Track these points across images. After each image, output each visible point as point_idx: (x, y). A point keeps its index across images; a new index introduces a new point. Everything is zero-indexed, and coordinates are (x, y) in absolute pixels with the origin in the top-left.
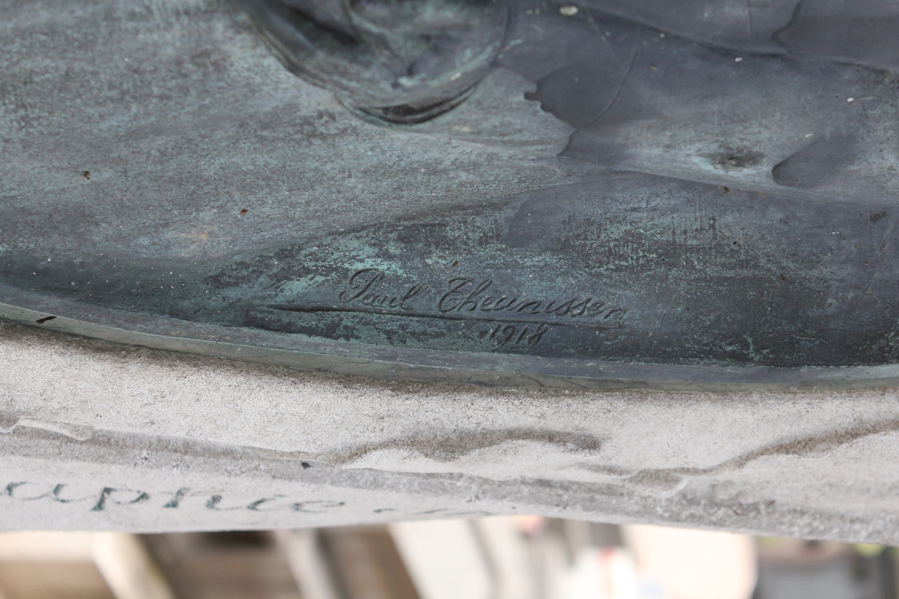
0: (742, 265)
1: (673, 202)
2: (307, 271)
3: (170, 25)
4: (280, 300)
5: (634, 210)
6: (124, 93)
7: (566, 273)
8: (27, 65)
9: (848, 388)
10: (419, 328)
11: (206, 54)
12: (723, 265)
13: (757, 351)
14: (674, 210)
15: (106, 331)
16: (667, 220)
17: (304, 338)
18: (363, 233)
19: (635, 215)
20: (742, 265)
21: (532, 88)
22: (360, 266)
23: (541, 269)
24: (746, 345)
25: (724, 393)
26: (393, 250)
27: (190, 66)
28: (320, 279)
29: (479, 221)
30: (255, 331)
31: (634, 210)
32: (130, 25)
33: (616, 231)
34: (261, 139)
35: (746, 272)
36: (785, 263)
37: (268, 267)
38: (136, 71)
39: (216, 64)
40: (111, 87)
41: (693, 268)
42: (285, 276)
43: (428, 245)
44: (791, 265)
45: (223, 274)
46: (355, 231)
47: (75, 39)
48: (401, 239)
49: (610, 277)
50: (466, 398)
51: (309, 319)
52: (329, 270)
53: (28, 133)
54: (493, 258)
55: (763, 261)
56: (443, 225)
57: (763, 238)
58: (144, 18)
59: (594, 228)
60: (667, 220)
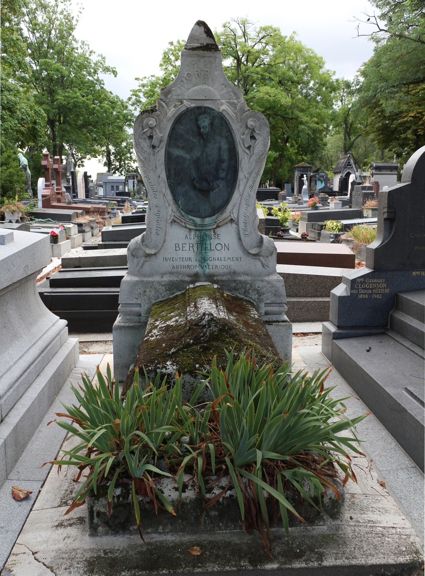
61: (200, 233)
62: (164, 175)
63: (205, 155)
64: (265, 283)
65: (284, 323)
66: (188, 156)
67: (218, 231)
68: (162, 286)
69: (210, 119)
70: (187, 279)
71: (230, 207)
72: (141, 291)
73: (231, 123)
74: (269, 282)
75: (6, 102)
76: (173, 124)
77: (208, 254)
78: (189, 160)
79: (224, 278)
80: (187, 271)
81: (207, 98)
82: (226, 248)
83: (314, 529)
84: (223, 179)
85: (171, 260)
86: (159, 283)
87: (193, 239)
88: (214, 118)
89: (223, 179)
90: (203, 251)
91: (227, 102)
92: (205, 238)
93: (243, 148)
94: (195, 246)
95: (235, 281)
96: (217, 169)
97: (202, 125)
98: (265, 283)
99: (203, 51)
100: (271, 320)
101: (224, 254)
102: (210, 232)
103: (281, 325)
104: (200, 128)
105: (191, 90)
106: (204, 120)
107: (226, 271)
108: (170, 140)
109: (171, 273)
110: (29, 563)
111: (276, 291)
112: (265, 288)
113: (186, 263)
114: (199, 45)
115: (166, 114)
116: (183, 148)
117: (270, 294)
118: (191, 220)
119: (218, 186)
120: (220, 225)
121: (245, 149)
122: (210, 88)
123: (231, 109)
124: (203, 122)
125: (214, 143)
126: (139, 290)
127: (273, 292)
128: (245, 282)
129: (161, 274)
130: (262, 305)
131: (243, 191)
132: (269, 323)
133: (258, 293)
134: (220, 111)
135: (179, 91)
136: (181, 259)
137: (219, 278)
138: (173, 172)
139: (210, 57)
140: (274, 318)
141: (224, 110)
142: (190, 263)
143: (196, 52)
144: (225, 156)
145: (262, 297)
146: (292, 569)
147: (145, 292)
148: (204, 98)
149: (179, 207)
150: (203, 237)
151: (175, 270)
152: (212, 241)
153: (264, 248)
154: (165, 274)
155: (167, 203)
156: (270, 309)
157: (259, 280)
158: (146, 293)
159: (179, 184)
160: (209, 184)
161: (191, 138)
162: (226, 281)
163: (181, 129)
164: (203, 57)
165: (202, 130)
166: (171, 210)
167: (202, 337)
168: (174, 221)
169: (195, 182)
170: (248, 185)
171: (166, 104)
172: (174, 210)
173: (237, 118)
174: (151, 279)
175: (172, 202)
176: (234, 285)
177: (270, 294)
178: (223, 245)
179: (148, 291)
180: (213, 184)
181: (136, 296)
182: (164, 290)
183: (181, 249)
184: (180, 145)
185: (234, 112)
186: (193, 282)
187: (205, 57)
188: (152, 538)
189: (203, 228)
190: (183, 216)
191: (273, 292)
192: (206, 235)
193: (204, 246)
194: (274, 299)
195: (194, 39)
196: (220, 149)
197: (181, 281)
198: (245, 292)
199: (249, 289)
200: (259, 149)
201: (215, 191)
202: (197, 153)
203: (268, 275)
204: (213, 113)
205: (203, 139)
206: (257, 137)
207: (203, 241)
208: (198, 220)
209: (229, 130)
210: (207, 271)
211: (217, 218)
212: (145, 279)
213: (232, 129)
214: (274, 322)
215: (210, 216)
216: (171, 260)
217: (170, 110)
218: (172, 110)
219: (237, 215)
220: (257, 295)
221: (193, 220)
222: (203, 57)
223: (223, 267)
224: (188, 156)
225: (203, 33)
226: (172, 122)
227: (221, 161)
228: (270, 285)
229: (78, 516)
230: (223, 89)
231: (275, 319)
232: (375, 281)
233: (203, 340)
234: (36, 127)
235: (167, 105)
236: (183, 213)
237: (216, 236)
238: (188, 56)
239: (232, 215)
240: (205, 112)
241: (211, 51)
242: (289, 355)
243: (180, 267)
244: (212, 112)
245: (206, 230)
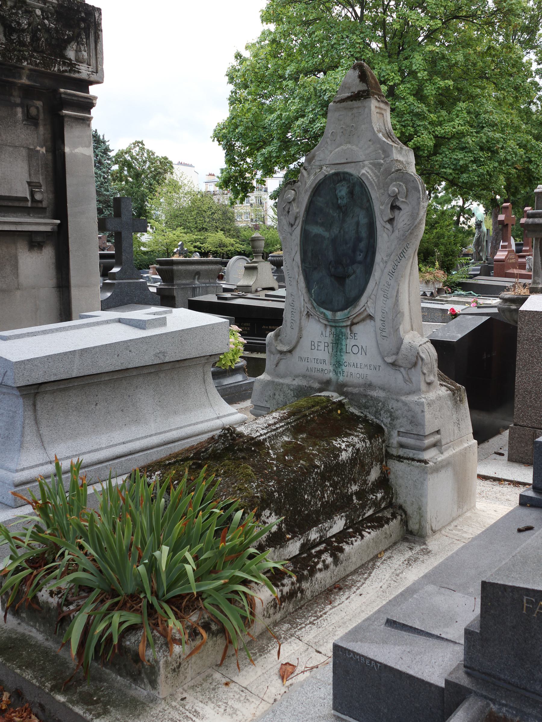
61: (336, 330)
62: (298, 258)
63: (342, 233)
64: (400, 404)
65: (419, 464)
66: (326, 234)
67: (356, 328)
68: (291, 390)
69: (348, 187)
70: (316, 385)
71: (363, 299)
72: (271, 393)
73: (370, 190)
74: (405, 404)
75: (484, 141)
76: (310, 196)
77: (344, 357)
78: (328, 238)
79: (356, 391)
80: (319, 375)
81: (349, 160)
82: (363, 353)
83: (136, 689)
84: (360, 263)
85: (306, 360)
86: (288, 385)
87: (327, 337)
88: (354, 185)
89: (360, 263)
90: (338, 353)
91: (371, 163)
92: (341, 336)
93: (382, 222)
94: (331, 345)
95: (366, 396)
96: (355, 249)
97: (339, 194)
98: (400, 404)
99: (352, 101)
100: (405, 456)
101: (360, 359)
102: (346, 330)
103: (413, 465)
105: (333, 153)
106: (341, 188)
107: (361, 381)
109: (304, 376)
111: (413, 417)
112: (399, 411)
113: (320, 366)
114: (349, 94)
116: (322, 225)
117: (405, 419)
118: (322, 313)
119: (354, 272)
120: (355, 321)
121: (384, 224)
122: (354, 147)
124: (340, 191)
125: (353, 217)
126: (269, 392)
127: (410, 417)
128: (377, 400)
129: (295, 376)
130: (395, 433)
131: (380, 278)
132: (400, 458)
133: (391, 416)
135: (322, 156)
136: (316, 360)
137: (350, 389)
138: (310, 255)
139: (358, 107)
140: (410, 453)
141: (363, 174)
142: (324, 367)
143: (344, 104)
144: (364, 233)
145: (394, 423)
146: (71, 710)
147: (275, 395)
148: (345, 161)
149: (311, 297)
150: (339, 336)
151: (308, 373)
152: (348, 341)
153: (400, 356)
154: (297, 376)
156: (404, 440)
157: (394, 399)
158: (275, 397)
159: (315, 269)
161: (331, 211)
162: (356, 394)
163: (320, 201)
164: (351, 109)
165: (339, 202)
167: (203, 452)
168: (308, 315)
169: (331, 267)
170: (386, 271)
172: (306, 300)
174: (281, 381)
175: (304, 290)
176: (364, 401)
177: (405, 419)
178: (360, 348)
179: (277, 394)
181: (267, 399)
182: (292, 395)
183: (316, 348)
184: (319, 221)
186: (321, 390)
187: (353, 108)
188: (31, 631)
189: (337, 325)
190: (314, 308)
191: (410, 417)
192: (342, 333)
193: (340, 346)
194: (409, 427)
195: (345, 88)
196: (358, 224)
197: (310, 387)
198: (376, 412)
199: (381, 409)
200: (404, 223)
201: (351, 278)
202: (335, 230)
203: (409, 393)
204: (352, 179)
206: (401, 206)
207: (338, 340)
208: (329, 314)
209: (369, 200)
210: (341, 378)
211: (349, 312)
212: (277, 380)
214: (408, 459)
215: (342, 310)
216: (306, 360)
220: (389, 419)
221: (324, 314)
222: (351, 109)
223: (358, 375)
224: (326, 234)
225: (357, 77)
226: (309, 193)
227: (359, 239)
228: (406, 408)
230: (369, 147)
231: (411, 455)
233: (203, 456)
234: (531, 167)
236: (315, 304)
237: (353, 335)
238: (335, 111)
240: (344, 179)
241: (360, 100)
242: (423, 509)
243: (314, 371)
245: (342, 327)
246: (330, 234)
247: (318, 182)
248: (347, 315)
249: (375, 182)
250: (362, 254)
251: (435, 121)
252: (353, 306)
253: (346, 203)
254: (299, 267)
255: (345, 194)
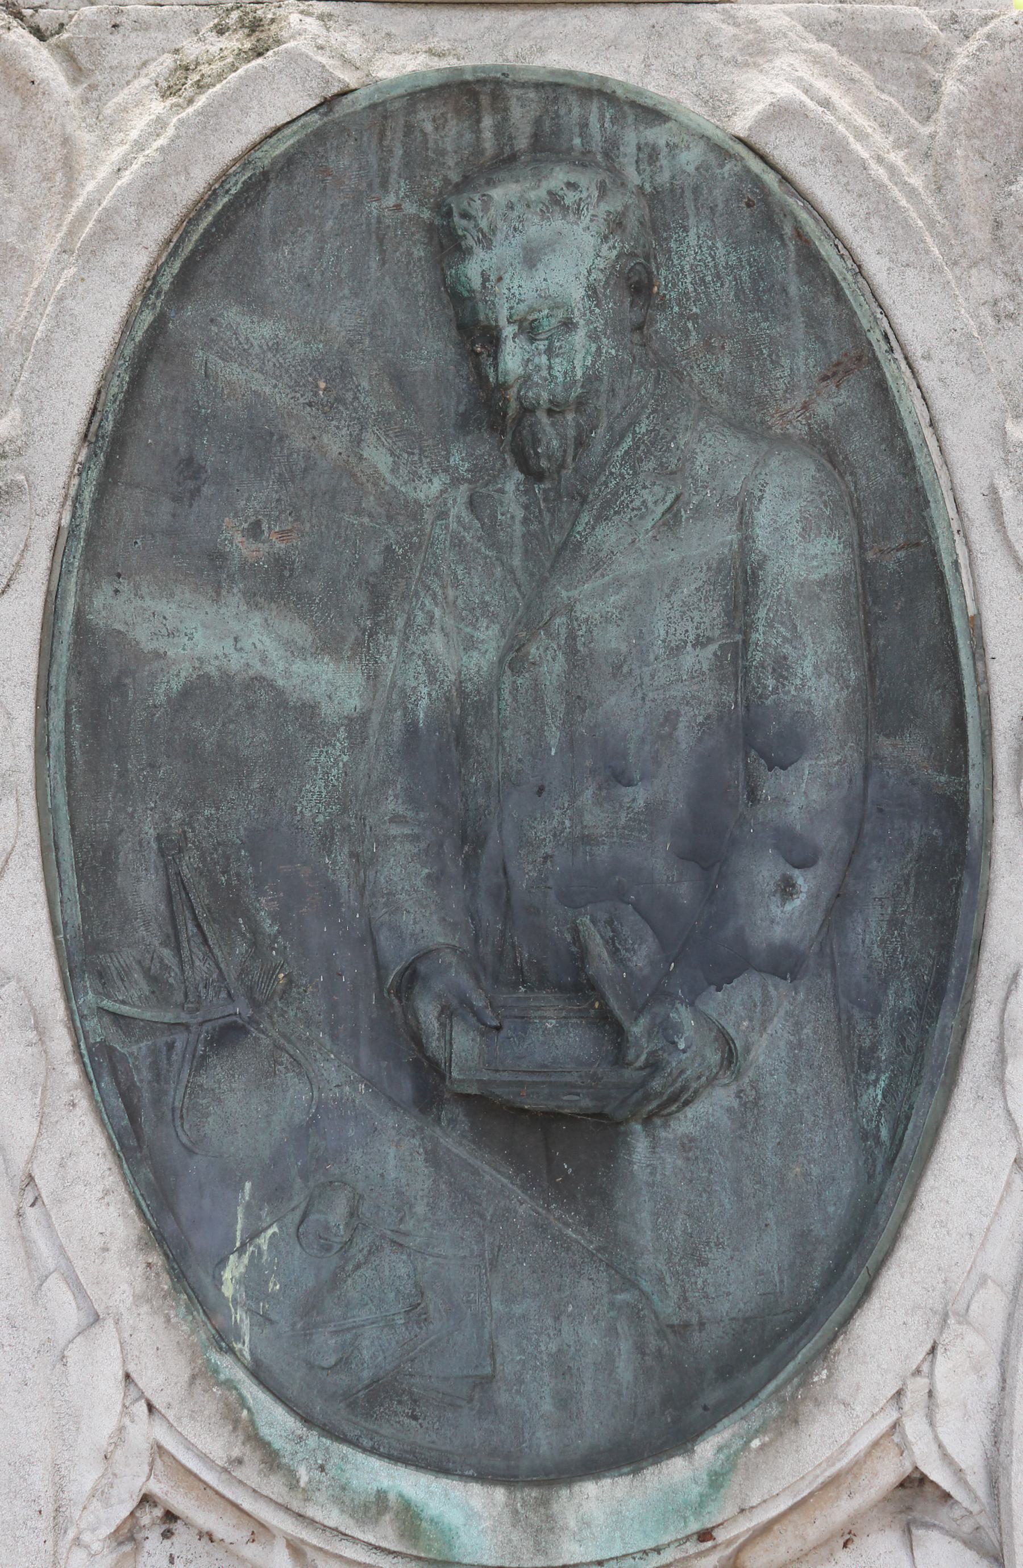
0: (907, 883)
1: (860, 920)
2: (877, 1126)
3: (661, 1157)
4: (888, 1144)
5: (863, 942)
6: (705, 1190)
7: (902, 982)
8: (678, 1233)
9: (988, 822)
10: (918, 1068)
11: (683, 1145)
12: (906, 894)
13: (957, 875)
14: (866, 921)
15: (883, 1242)
16: (873, 924)
17: (908, 1132)
18: (859, 1092)
19: (867, 941)
20: (907, 883)
21: (713, 988)
22: (880, 1097)
23: (897, 996)
24: (953, 882)
25: (987, 893)
26: (873, 1077)
27: (691, 1154)
28: (883, 1120)
29: (860, 1027)
30: (898, 1159)
31: (863, 942)
32: (658, 1177)
33: (877, 952)
34: (754, 1129)
35: (912, 881)
36: (908, 859)
37: (871, 1147)
38: (691, 1181)
39: (690, 1141)
40: (701, 1196)
41: (906, 911)
42: (877, 1138)
43: (873, 1058)
44: (910, 855)
45: (868, 1173)
46: (855, 1096)
47: (664, 1205)
48: (867, 1072)
49: (907, 958)
50: (968, 1046)
51: (900, 1130)
52: (879, 1114)
53: (728, 1245)
54: (886, 1022)
55: (906, 871)
56: (860, 1048)
57: (890, 871)
58: (655, 1168)
59: (874, 965)
60: (873, 924)
69: (616, 224)
73: (876, 266)
76: (148, 290)
91: (822, 29)
104: (493, 339)
106: (536, 229)
108: (103, 489)
110: (40, 1512)
115: (69, 166)
123: (869, 108)
124: (531, 258)
125: (671, 519)
134: (741, 125)
155: (58, 1291)
160: (618, 1033)
166: (111, 1388)
171: (68, 56)
172: (149, 1381)
173: (953, 212)
180: (667, 1031)
185: (907, 141)
204: (650, 155)
205: (534, 475)
211: (717, 1480)
213: (891, 337)
217: (117, 123)
218: (138, 124)
219: (979, 1427)
229: (591, 124)
232: (847, 292)
235: (77, 72)
239: (915, 1427)
244: (630, 139)
246: (373, 678)
247: (244, 159)
248: (700, 1505)
249: (911, 193)
250: (803, 881)
251: (64, 175)
252: (755, 1412)
253: (591, 379)
254: (40, 1030)
255: (577, 293)
